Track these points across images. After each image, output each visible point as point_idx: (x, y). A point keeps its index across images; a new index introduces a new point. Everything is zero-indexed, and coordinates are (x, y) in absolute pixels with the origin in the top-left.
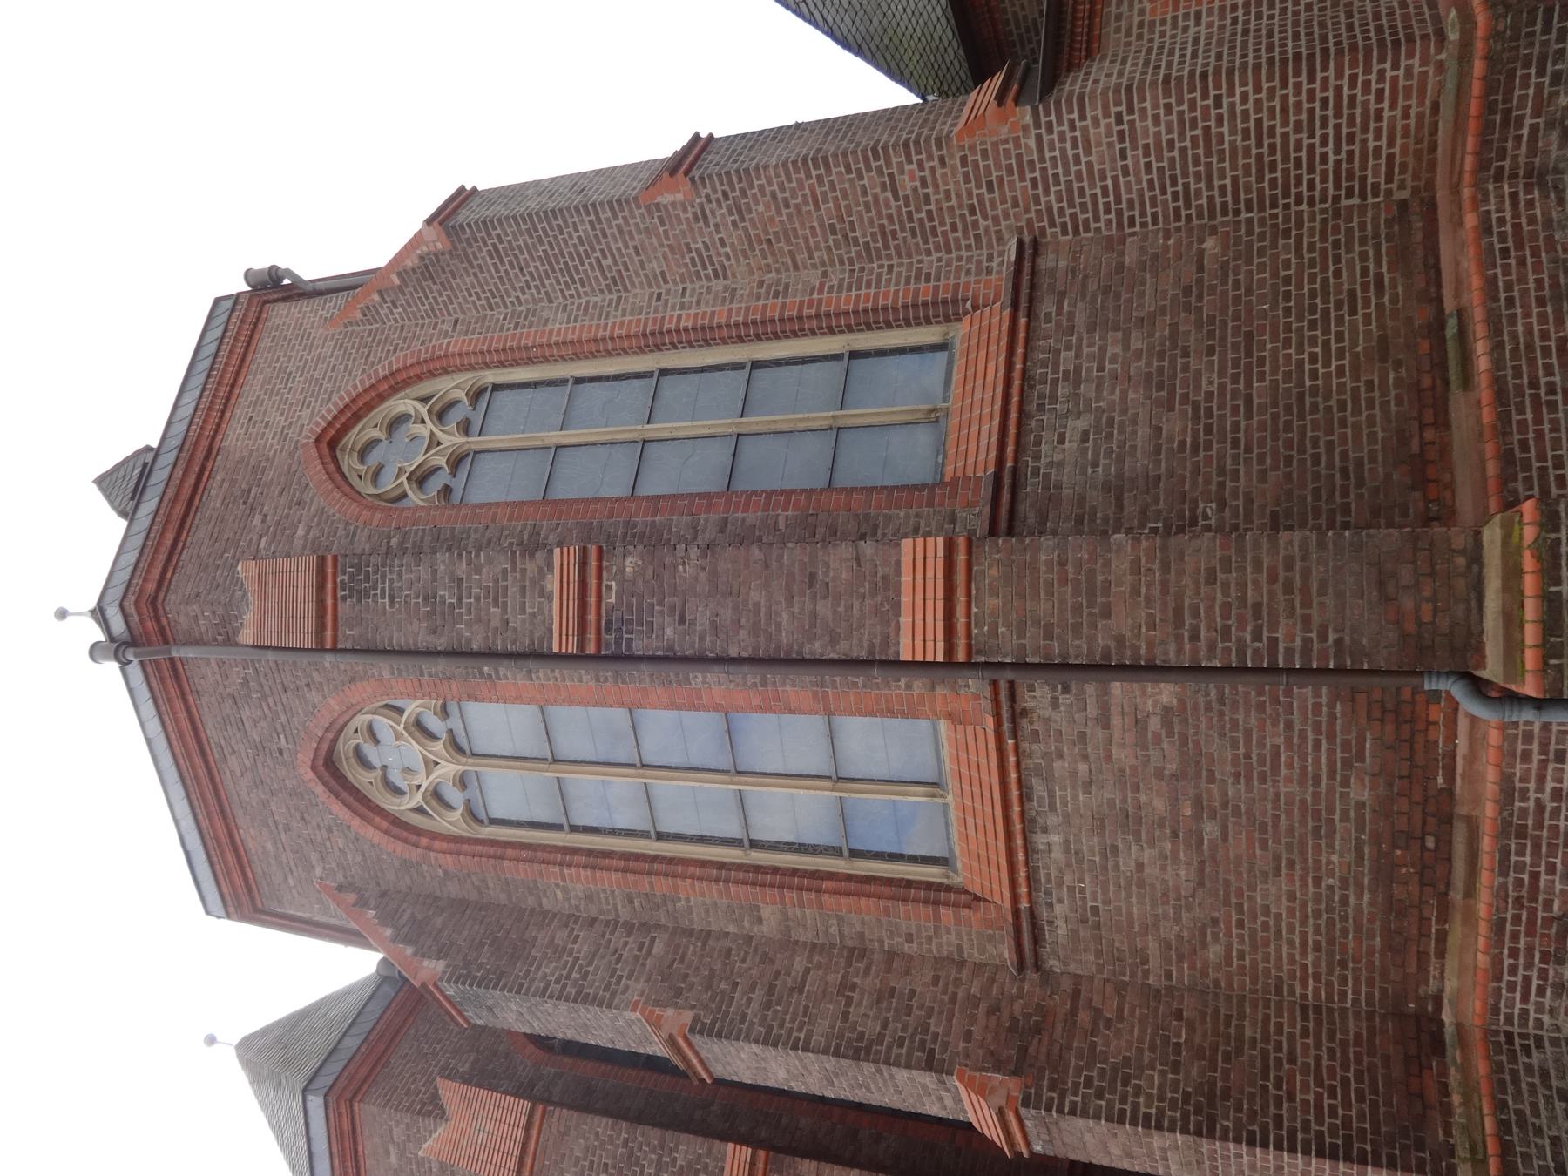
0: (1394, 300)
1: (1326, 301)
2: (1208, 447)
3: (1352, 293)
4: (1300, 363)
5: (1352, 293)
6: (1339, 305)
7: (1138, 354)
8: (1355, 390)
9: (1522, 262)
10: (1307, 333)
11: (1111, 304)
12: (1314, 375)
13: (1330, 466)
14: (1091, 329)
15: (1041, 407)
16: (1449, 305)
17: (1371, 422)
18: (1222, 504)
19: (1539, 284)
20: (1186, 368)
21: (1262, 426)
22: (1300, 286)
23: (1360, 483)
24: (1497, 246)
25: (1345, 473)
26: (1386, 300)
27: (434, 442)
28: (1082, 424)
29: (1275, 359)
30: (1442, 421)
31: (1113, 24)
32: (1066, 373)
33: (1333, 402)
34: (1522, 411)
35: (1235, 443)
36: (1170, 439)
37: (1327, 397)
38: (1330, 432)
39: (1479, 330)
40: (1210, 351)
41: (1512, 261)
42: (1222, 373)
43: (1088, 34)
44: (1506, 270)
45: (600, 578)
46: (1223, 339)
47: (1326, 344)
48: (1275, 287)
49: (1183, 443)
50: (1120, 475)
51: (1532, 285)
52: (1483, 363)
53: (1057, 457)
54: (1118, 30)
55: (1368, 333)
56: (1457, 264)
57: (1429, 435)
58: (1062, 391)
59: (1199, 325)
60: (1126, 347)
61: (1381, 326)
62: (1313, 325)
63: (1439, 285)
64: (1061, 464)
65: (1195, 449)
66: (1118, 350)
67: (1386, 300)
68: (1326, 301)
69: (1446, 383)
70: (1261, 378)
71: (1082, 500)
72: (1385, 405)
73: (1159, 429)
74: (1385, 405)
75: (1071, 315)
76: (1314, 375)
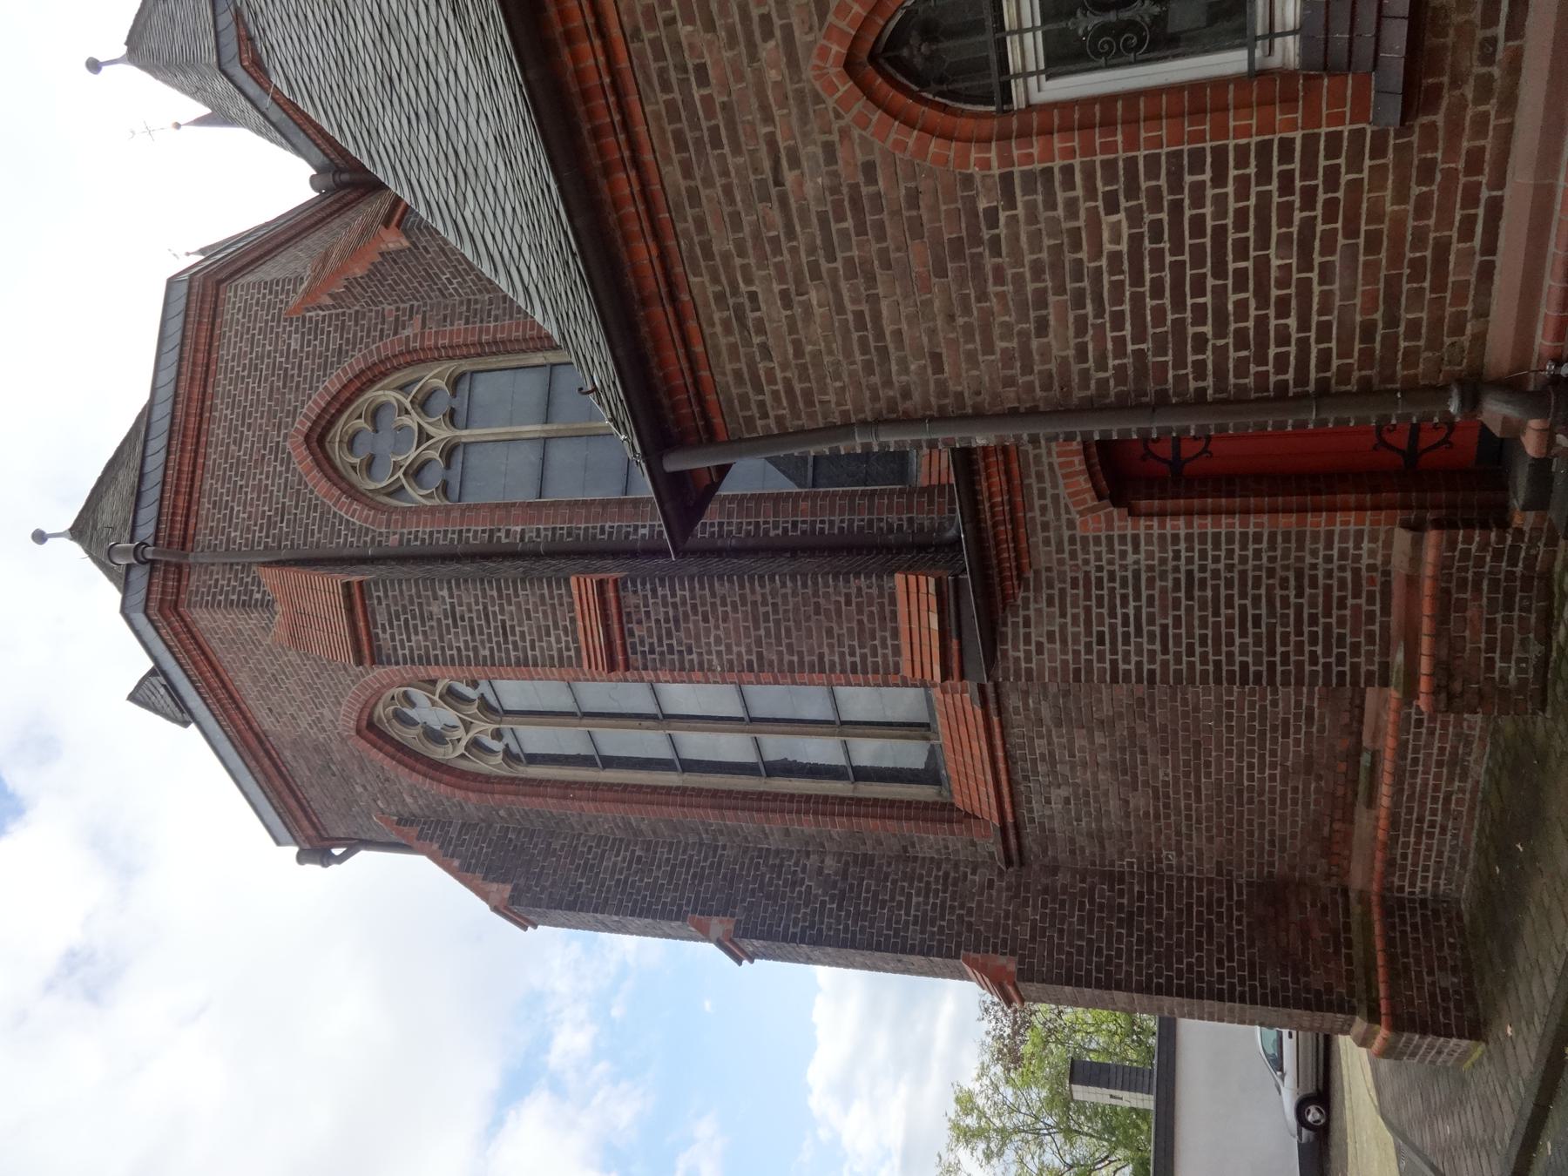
0: (1321, 730)
1: (1262, 723)
2: (1167, 817)
3: (1286, 722)
4: (1240, 770)
5: (1286, 722)
6: (1274, 729)
7: (1103, 747)
8: (1283, 793)
9: (1431, 732)
10: (1246, 748)
11: (1071, 705)
12: (1251, 778)
13: (1262, 837)
14: (1058, 723)
15: (1026, 778)
16: (1366, 741)
17: (1294, 814)
18: (1180, 854)
19: (1442, 750)
20: (1145, 762)
21: (1209, 809)
22: (1241, 710)
24: (1414, 717)
25: (1272, 843)
26: (1314, 729)
27: (424, 436)
28: (1064, 792)
29: (1219, 765)
30: (1348, 819)
31: (1041, 535)
32: (1042, 755)
33: (1265, 798)
34: (1407, 835)
35: (1189, 817)
36: (1137, 809)
37: (1261, 794)
38: (1262, 816)
39: (1387, 765)
40: (1165, 752)
41: (1424, 730)
42: (1175, 769)
43: (1015, 549)
44: (1417, 736)
45: (623, 638)
46: (1175, 743)
47: (1262, 757)
48: (1219, 708)
49: (1147, 814)
50: (1100, 829)
51: (1435, 751)
52: (1385, 801)
53: (1048, 812)
54: (1047, 542)
55: (1297, 753)
56: (1378, 715)
57: (1337, 826)
58: (1041, 768)
59: (1153, 730)
60: (1092, 742)
61: (1308, 748)
62: (1251, 742)
63: (1361, 722)
64: (1051, 817)
65: (1157, 817)
66: (1085, 743)
67: (1314, 729)
68: (1262, 723)
70: (1208, 775)
71: (1072, 841)
72: (1306, 805)
73: (1127, 802)
74: (1306, 805)
75: (1037, 711)
76: (1251, 778)
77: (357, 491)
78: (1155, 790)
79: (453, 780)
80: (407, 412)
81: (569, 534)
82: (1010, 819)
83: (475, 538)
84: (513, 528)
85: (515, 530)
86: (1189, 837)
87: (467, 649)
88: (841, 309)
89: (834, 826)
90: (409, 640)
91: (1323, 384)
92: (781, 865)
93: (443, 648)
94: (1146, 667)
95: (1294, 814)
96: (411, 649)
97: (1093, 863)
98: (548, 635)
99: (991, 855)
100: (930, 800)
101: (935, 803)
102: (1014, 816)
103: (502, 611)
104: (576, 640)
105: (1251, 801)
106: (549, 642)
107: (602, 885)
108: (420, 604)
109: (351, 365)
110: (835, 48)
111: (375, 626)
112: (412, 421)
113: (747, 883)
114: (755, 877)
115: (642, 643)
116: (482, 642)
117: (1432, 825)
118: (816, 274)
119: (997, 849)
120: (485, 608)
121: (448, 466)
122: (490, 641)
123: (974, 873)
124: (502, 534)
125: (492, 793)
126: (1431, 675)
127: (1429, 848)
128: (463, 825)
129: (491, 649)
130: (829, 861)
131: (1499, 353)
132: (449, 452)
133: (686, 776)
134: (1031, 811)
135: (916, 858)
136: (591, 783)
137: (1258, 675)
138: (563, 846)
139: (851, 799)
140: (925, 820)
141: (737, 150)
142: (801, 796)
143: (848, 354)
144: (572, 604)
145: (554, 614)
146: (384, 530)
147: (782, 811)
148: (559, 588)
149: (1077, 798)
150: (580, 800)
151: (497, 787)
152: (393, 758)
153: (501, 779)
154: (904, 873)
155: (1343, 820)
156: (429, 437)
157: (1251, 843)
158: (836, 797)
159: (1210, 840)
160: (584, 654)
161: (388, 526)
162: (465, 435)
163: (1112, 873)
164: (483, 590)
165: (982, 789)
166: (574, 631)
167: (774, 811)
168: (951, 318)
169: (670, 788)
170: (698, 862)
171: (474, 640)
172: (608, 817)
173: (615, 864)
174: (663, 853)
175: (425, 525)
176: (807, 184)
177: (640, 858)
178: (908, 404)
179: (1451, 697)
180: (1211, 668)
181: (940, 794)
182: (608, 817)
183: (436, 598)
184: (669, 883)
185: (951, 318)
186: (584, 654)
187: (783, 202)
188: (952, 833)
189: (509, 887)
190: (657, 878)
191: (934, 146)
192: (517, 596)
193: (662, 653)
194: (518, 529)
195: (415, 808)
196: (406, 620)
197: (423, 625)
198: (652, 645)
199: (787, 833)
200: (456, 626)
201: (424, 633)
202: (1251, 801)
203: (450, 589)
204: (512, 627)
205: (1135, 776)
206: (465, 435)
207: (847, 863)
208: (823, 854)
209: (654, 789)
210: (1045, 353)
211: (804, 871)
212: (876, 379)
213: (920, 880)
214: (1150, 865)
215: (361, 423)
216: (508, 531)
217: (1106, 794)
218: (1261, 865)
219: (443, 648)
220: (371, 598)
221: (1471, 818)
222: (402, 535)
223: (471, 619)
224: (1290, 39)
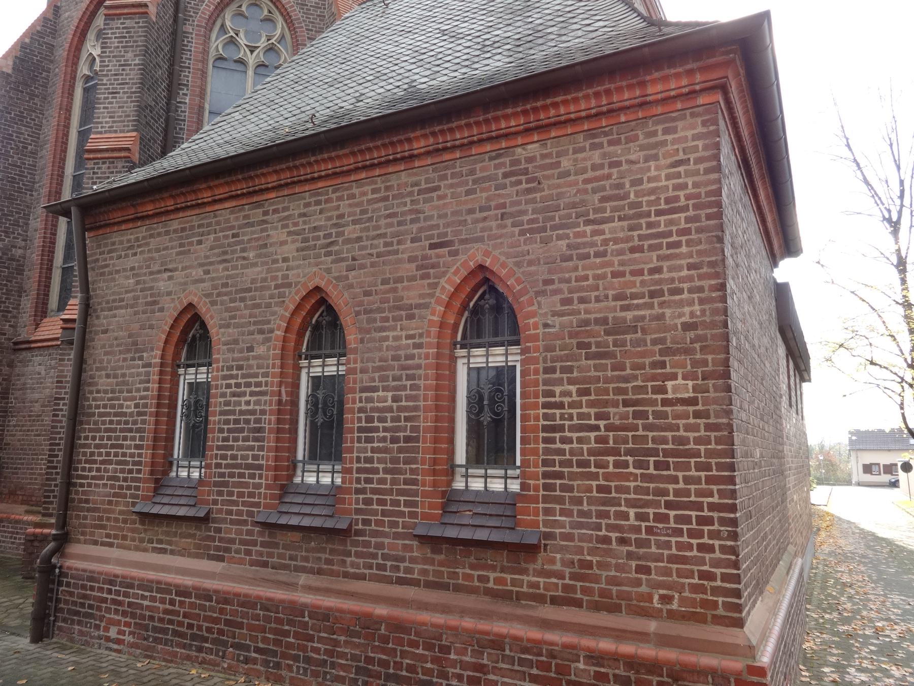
2: (30, 421)
13: (18, 464)
17: (27, 479)
18: (15, 426)
23: (13, 473)
25: (16, 468)
27: (252, 50)
28: (43, 373)
30: (23, 503)
34: (12, 527)
35: (28, 431)
49: (31, 411)
64: (33, 366)
65: (29, 416)
69: (32, 506)
71: (23, 375)
72: (30, 484)
73: (37, 402)
77: (222, 10)
78: (40, 416)
79: (75, 43)
80: (268, 40)
81: (181, 129)
82: (33, 345)
83: (185, 76)
84: (188, 98)
85: (186, 98)
86: (21, 431)
87: (108, 71)
88: (127, 292)
89: (37, 255)
90: (116, 38)
91: (75, 485)
92: (19, 226)
93: (109, 57)
94: (60, 413)
95: (27, 479)
96: (110, 38)
97: (13, 385)
98: (110, 117)
99: (19, 335)
100: (49, 306)
101: (47, 308)
102: (34, 348)
103: (124, 93)
104: (106, 132)
105: (33, 459)
106: (105, 117)
107: (9, 126)
108: (132, 46)
109: (295, 10)
110: (196, 299)
111: (125, 19)
112: (262, 43)
113: (8, 207)
114: (12, 212)
115: (99, 168)
116: (110, 80)
117: (15, 538)
118: (138, 283)
119: (21, 338)
120: (127, 83)
121: (236, 61)
122: (111, 84)
123: (10, 326)
124: (185, 92)
125: (66, 66)
126: (42, 534)
127: (6, 537)
128: (53, 46)
129: (106, 84)
130: (20, 252)
131: (75, 549)
132: (241, 62)
133: (71, 177)
134: (37, 356)
135: (21, 297)
136: (69, 124)
137: (52, 462)
138: (36, 104)
139: (52, 265)
140: (37, 303)
141: (178, 254)
142: (55, 239)
143: (114, 293)
144: (123, 131)
145: (120, 122)
146: (196, 23)
147: (45, 228)
148: (133, 126)
149: (40, 378)
150: (59, 117)
151: (69, 69)
152: (87, 9)
153: (74, 72)
154: (12, 291)
155: (22, 500)
156: (252, 52)
157: (16, 459)
158: (53, 257)
159: (19, 440)
160: (98, 136)
161: (197, 26)
162: (250, 72)
163: (8, 393)
164: (136, 84)
165: (47, 333)
166: (110, 132)
167: (46, 224)
168: (116, 339)
169: (63, 168)
170: (22, 181)
171: (112, 75)
172: (49, 132)
173: (22, 134)
174: (29, 161)
175: (196, 47)
176: (162, 285)
177: (27, 148)
178: (94, 318)
179: (32, 541)
180: (57, 442)
181: (52, 311)
182: (49, 132)
183: (135, 56)
184: (9, 164)
185: (116, 339)
186: (98, 136)
187: (159, 272)
188: (30, 316)
189: (10, 71)
190: (13, 157)
191: (164, 337)
192: (131, 102)
193: (92, 178)
194: (187, 101)
195: (62, 18)
196: (125, 37)
197: (122, 47)
198: (97, 173)
199: (36, 230)
200: (120, 65)
201: (118, 47)
202: (33, 459)
203: (139, 65)
204: (115, 98)
205: (46, 406)
206: (250, 72)
207: (18, 261)
208: (25, 248)
209: (63, 160)
210: (100, 377)
211: (14, 238)
212: (104, 305)
213: (6, 299)
214: (11, 412)
215: (266, 12)
216: (186, 95)
217: (40, 393)
218: (7, 463)
219: (109, 57)
220: (139, 18)
221: (17, 555)
222: (192, 33)
223: (122, 75)
224: (464, 484)
